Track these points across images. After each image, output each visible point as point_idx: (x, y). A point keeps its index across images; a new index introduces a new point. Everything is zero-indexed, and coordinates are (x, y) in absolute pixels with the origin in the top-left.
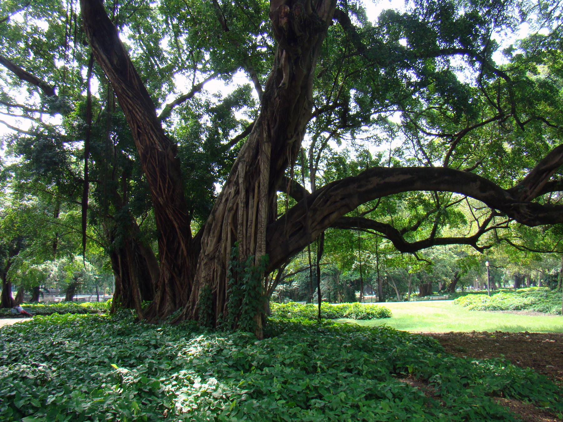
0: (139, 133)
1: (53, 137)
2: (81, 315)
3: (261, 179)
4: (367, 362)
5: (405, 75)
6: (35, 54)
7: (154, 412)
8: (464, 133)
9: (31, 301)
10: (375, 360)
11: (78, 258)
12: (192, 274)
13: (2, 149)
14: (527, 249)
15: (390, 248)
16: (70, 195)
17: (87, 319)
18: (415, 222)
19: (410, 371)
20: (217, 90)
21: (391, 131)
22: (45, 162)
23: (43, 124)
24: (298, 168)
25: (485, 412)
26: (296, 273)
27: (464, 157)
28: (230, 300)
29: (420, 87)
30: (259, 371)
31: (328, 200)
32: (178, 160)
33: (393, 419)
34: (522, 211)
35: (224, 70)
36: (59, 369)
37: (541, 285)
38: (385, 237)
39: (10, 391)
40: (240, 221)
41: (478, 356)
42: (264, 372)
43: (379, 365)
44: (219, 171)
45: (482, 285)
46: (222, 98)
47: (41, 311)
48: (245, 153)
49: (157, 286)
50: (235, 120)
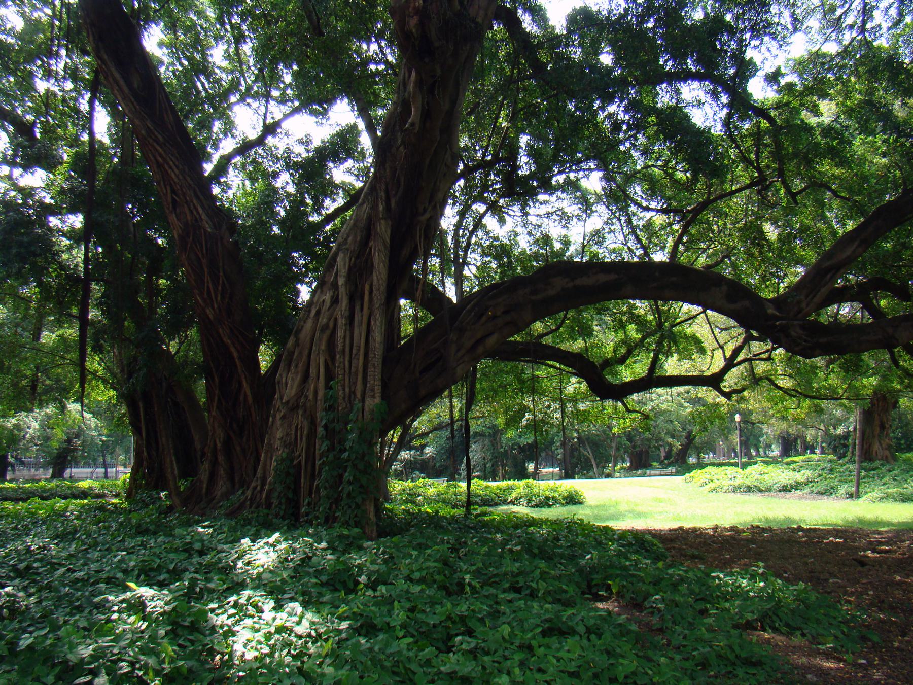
0: (174, 202)
2: (78, 501)
3: (375, 278)
4: (545, 576)
7: (199, 660)
8: (703, 206)
10: (558, 572)
11: (73, 407)
14: (800, 393)
15: (583, 393)
18: (623, 351)
21: (585, 203)
24: (435, 261)
25: (734, 654)
26: (431, 432)
27: (703, 246)
28: (324, 475)
30: (370, 593)
34: (793, 334)
35: (314, 99)
36: (39, 590)
37: (823, 452)
40: (340, 347)
41: (724, 566)
42: (378, 593)
44: (306, 266)
45: (729, 451)
46: (312, 147)
47: (11, 494)
48: (348, 236)
49: (203, 454)
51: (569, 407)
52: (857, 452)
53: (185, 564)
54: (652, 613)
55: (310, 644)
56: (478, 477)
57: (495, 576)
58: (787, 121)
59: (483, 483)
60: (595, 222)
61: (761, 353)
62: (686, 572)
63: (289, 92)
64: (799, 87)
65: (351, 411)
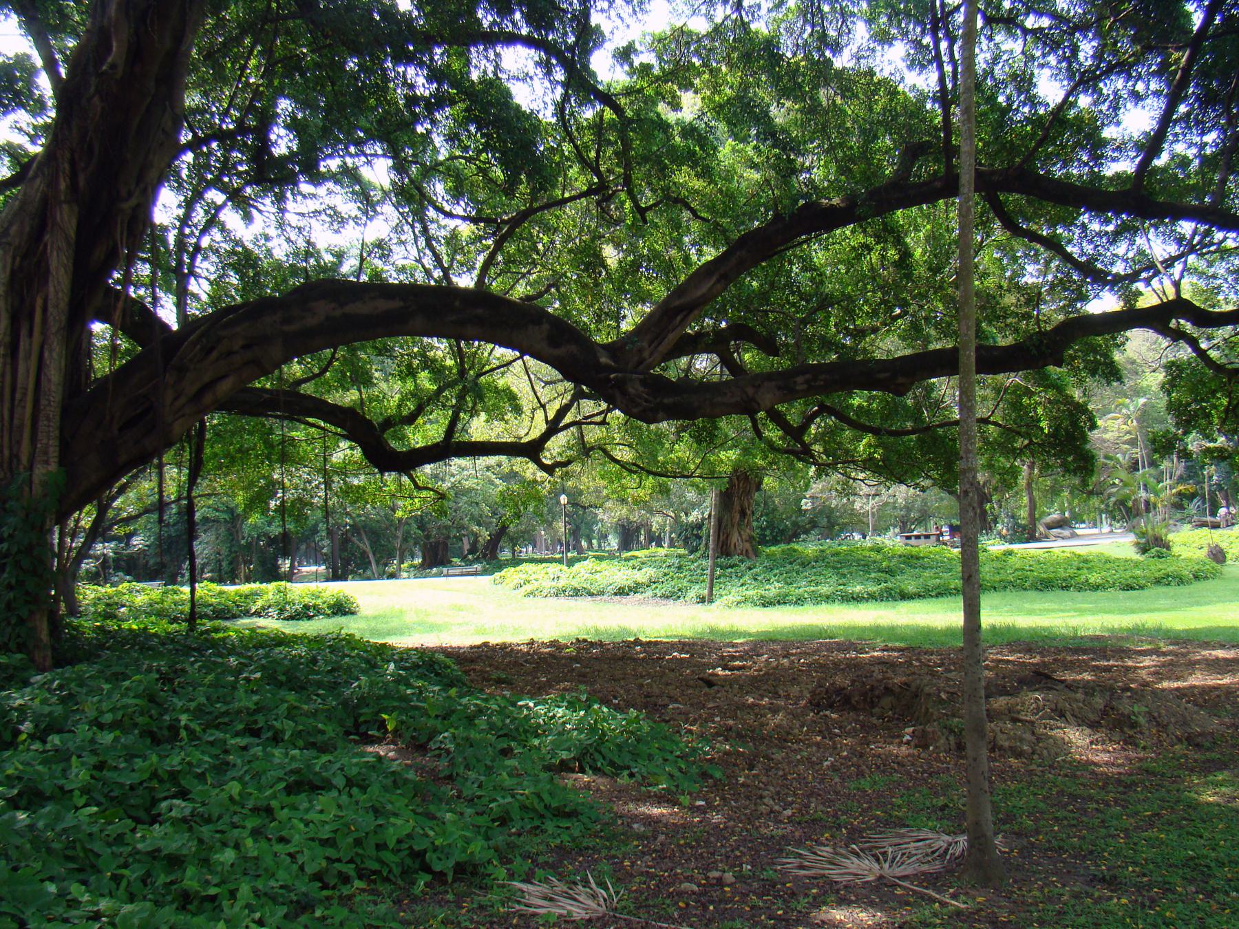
3: (51, 289)
4: (295, 712)
10: (313, 706)
14: (642, 469)
15: (356, 462)
18: (411, 405)
19: (389, 728)
21: (366, 199)
25: (542, 804)
30: (37, 746)
31: (212, 349)
33: (346, 830)
34: (631, 390)
37: (672, 545)
38: (345, 437)
41: (537, 691)
42: (48, 746)
43: (322, 718)
45: (553, 544)
48: (11, 224)
57: (227, 713)
58: (637, 113)
60: (379, 229)
61: (593, 415)
62: (486, 700)
64: (656, 71)
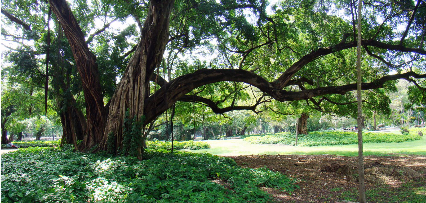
0: (75, 50)
1: (30, 52)
2: (44, 148)
5: (219, 19)
6: (20, 7)
7: (83, 200)
8: (250, 50)
9: (18, 140)
11: (43, 117)
12: (104, 125)
13: (2, 58)
16: (39, 83)
17: (48, 150)
18: (224, 98)
20: (118, 26)
22: (25, 66)
23: (24, 45)
24: (161, 69)
26: (160, 125)
27: (250, 63)
28: (124, 139)
29: (227, 25)
30: (140, 178)
32: (97, 64)
35: (121, 15)
36: (32, 177)
39: (6, 189)
40: (130, 97)
41: (254, 167)
42: (142, 178)
44: (119, 71)
46: (121, 31)
47: (23, 145)
49: (85, 132)
50: (127, 43)
51: (206, 117)
52: (297, 131)
53: (78, 169)
54: (230, 183)
55: (120, 195)
56: (176, 140)
59: (177, 142)
63: (113, 14)
65: (133, 118)
